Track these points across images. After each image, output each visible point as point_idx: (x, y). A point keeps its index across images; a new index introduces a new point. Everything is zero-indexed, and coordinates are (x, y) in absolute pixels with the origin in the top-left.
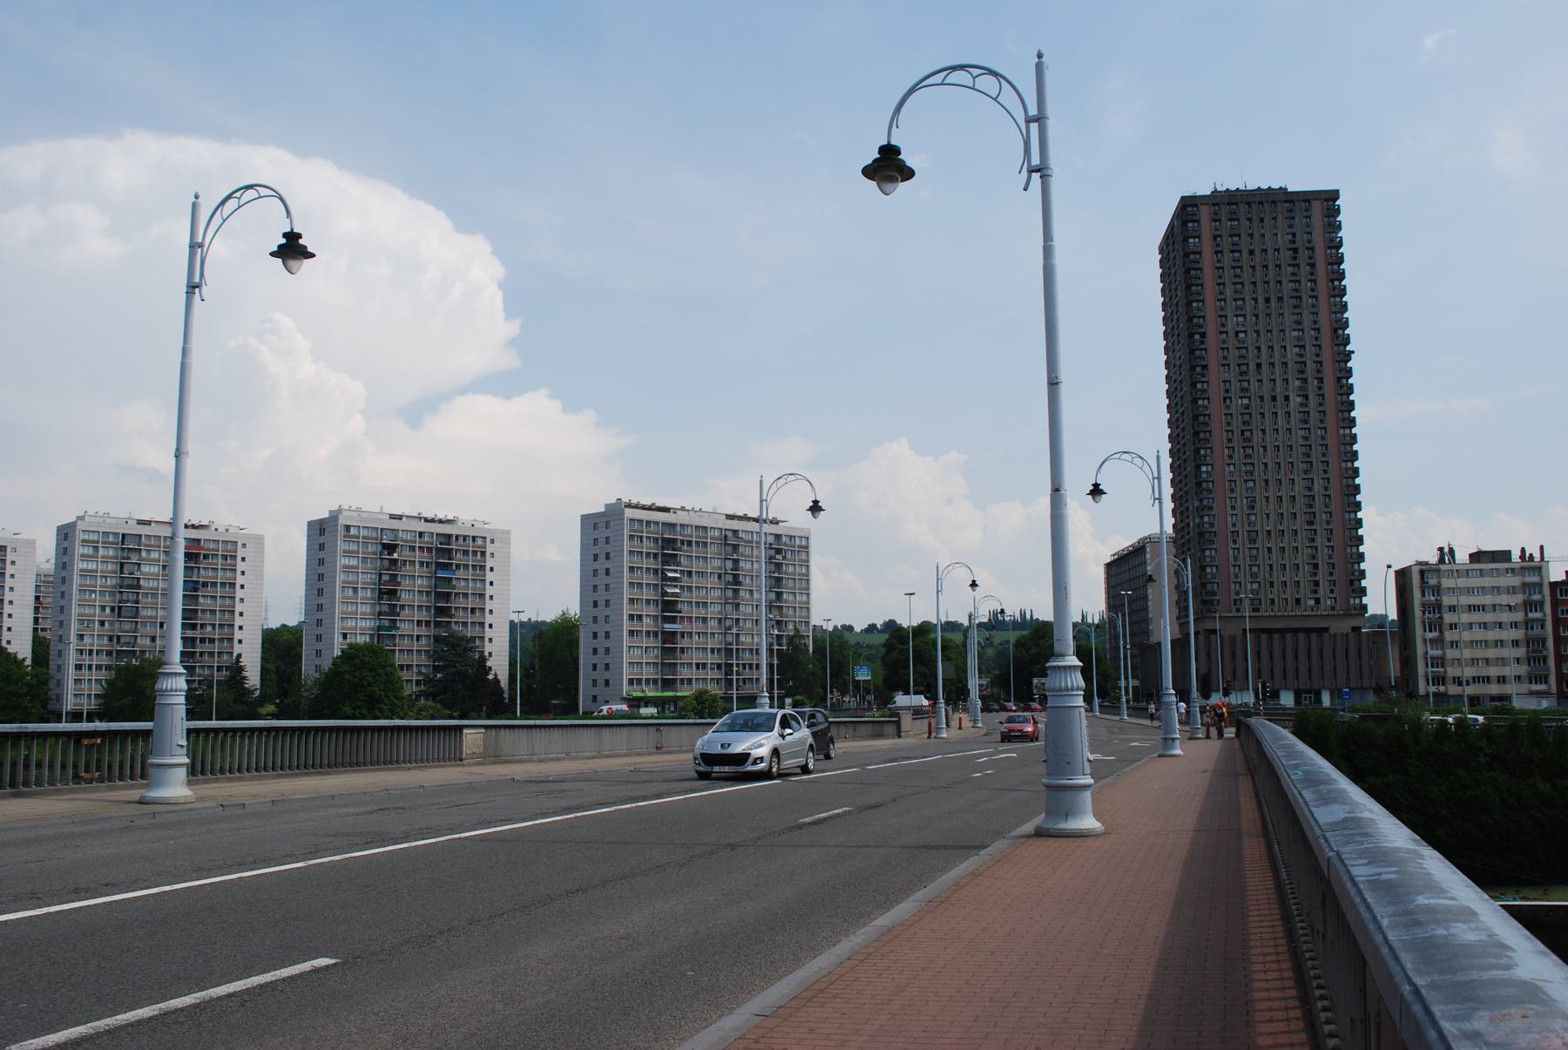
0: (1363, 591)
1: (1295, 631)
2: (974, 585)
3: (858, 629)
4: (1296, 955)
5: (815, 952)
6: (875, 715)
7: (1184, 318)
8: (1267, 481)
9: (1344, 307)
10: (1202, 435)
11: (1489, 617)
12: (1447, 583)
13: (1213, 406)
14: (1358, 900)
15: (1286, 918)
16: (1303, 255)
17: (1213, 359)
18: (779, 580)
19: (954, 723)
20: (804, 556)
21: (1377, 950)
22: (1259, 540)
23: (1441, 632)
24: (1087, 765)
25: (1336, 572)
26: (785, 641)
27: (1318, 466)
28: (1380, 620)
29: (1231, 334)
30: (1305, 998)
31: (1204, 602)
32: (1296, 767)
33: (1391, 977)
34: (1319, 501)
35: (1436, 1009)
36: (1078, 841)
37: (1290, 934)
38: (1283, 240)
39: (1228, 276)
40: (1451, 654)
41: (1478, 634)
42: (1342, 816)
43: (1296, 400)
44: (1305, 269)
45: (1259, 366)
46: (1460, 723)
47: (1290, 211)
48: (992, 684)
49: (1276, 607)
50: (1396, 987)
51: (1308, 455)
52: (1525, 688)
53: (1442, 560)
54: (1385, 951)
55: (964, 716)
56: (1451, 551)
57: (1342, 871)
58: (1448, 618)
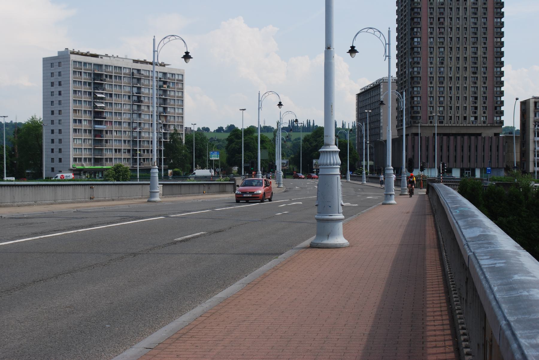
0: (502, 113)
1: (463, 135)
2: (280, 104)
3: (212, 130)
5: (181, 312)
8: (451, 48)
10: (415, 20)
15: (447, 292)
18: (165, 100)
20: (180, 86)
21: (490, 303)
22: (445, 82)
24: (341, 208)
25: (487, 102)
26: (168, 136)
27: (481, 40)
28: (510, 130)
30: (455, 335)
31: (412, 118)
32: (456, 208)
35: (518, 333)
36: (334, 251)
37: (449, 301)
48: (290, 163)
49: (453, 121)
50: (498, 322)
51: (476, 34)
54: (494, 303)
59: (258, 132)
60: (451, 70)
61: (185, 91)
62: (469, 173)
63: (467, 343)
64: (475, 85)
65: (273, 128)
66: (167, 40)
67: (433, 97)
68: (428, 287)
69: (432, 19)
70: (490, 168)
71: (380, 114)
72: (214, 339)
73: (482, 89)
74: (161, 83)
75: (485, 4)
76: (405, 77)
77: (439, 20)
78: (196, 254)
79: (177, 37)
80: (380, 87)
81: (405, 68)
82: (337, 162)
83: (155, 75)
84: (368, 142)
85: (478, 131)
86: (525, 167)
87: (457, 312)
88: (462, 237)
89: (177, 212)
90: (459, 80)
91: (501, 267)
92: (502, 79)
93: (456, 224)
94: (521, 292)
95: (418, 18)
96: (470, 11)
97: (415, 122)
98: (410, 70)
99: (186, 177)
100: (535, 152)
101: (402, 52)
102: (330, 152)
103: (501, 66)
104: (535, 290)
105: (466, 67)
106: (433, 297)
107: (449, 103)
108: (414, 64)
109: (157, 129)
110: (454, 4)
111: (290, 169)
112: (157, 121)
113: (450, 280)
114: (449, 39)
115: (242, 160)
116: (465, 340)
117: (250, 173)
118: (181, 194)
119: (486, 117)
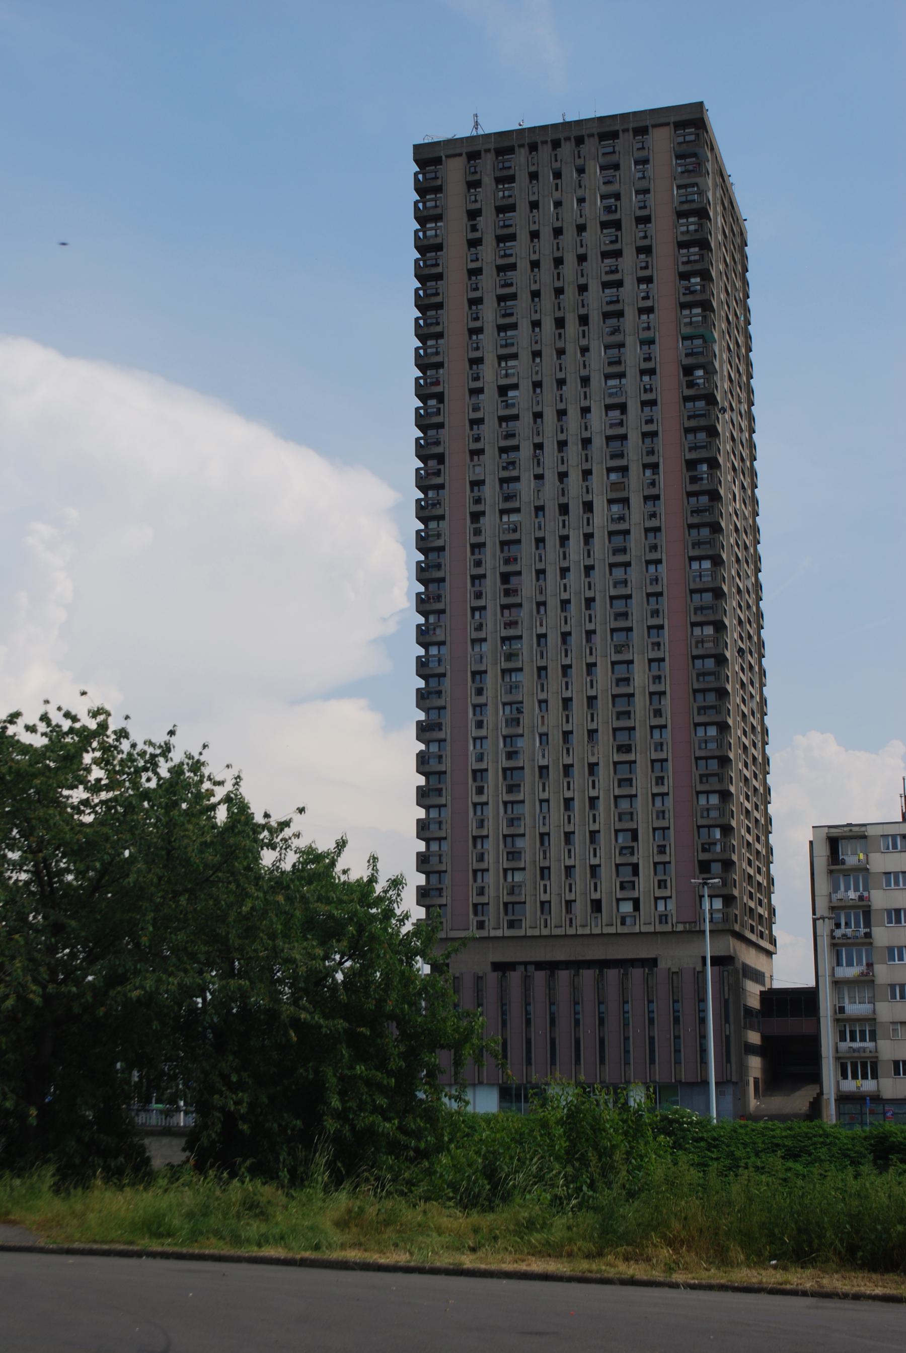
38: (595, 209)
49: (554, 920)
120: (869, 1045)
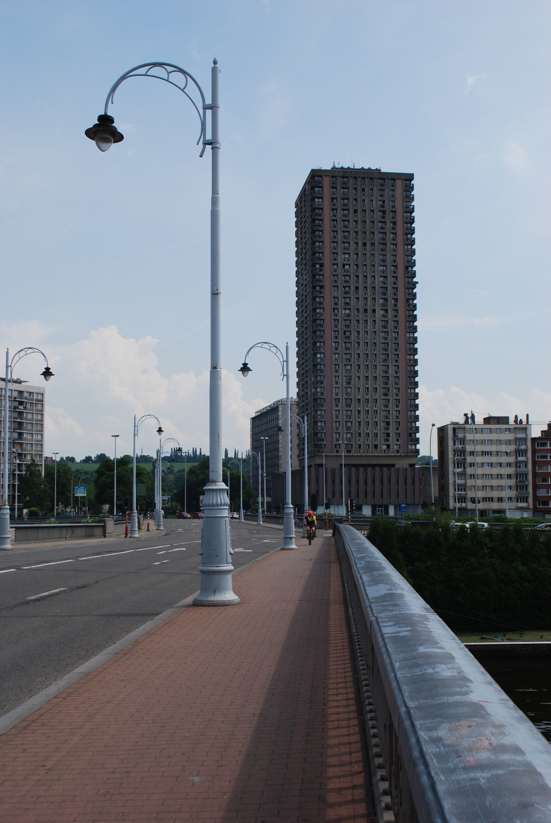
0: (417, 441)
1: (374, 466)
2: (160, 430)
3: (78, 460)
4: (357, 683)
5: (31, 693)
6: (89, 521)
7: (309, 253)
8: (359, 366)
9: (413, 252)
10: (318, 333)
11: (494, 459)
12: (469, 437)
13: (327, 314)
14: (384, 650)
15: (353, 658)
16: (389, 215)
17: (327, 282)
18: (20, 424)
19: (144, 527)
20: (39, 407)
21: (390, 683)
22: (353, 405)
23: (464, 468)
24: (229, 557)
25: (400, 428)
26: (24, 468)
27: (392, 357)
28: (427, 460)
29: (340, 265)
30: (361, 712)
31: (316, 446)
32: (362, 558)
33: (395, 701)
34: (391, 380)
35: (417, 723)
36: (222, 609)
37: (355, 669)
38: (376, 204)
39: (340, 226)
40: (470, 482)
41: (487, 470)
42: (383, 592)
43: (380, 313)
44: (389, 225)
45: (357, 288)
46: (474, 528)
47: (382, 185)
48: (172, 499)
49: (362, 450)
50: (397, 708)
51: (386, 350)
52: (514, 505)
53: (466, 422)
54: (394, 684)
55: (151, 522)
56: (473, 416)
57: (377, 629)
58: (469, 459)
59: (132, 463)
60: (359, 390)
61: (46, 413)
62: (382, 510)
63: (374, 722)
64: (386, 409)
65: (152, 458)
66: (23, 353)
67: (339, 422)
68: (331, 652)
69: (337, 333)
70: (404, 505)
71: (278, 441)
72: (70, 727)
73: (395, 413)
74: (16, 404)
75: (395, 316)
76: (307, 399)
77: (345, 334)
78: (53, 616)
79: (35, 350)
80: (278, 411)
81: (307, 388)
82: (225, 503)
83: (8, 393)
84: (265, 475)
85: (391, 462)
86: (444, 502)
87: (364, 683)
88: (365, 597)
89: (31, 562)
90: (368, 402)
91: (406, 636)
92: (417, 402)
93: (360, 579)
94: (424, 669)
95: (320, 331)
96: (379, 324)
97: (318, 452)
98: (313, 390)
99: (44, 518)
100: (455, 485)
101: (303, 369)
102: (216, 490)
103: (415, 387)
104: (442, 665)
105: (376, 388)
106: (337, 665)
107: (357, 429)
108: (317, 383)
109: (9, 460)
110: (361, 316)
111: (172, 507)
112: (9, 449)
113: (357, 644)
114: (356, 356)
115: (114, 496)
116: (372, 719)
117: (124, 512)
118: (37, 540)
119: (400, 445)
120: (463, 492)
